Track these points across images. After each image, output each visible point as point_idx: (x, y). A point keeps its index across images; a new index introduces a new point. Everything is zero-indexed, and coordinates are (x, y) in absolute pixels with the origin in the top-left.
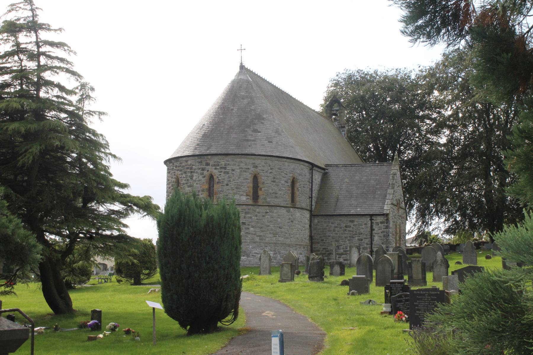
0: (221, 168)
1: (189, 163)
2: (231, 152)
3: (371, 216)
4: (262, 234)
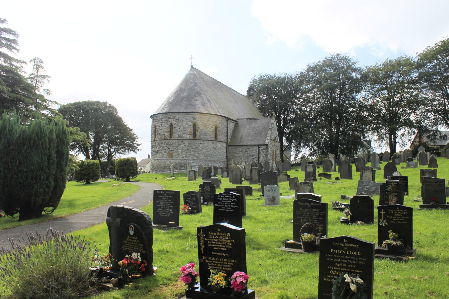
0: (176, 120)
1: (161, 117)
2: (181, 111)
3: (259, 145)
4: (198, 155)
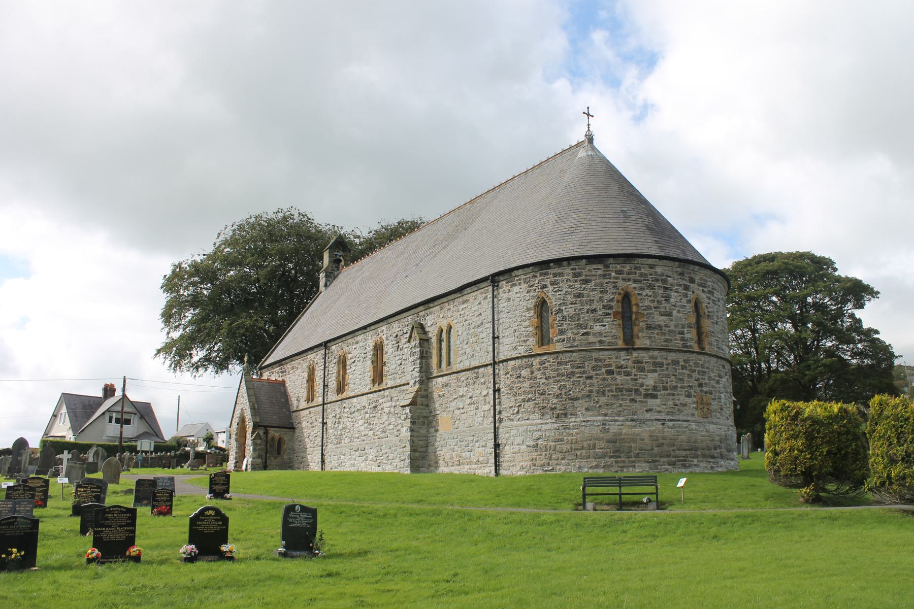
1: (659, 270)
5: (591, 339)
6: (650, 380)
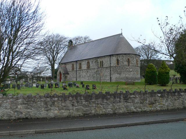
1: (133, 56)
5: (124, 64)
6: (131, 70)
